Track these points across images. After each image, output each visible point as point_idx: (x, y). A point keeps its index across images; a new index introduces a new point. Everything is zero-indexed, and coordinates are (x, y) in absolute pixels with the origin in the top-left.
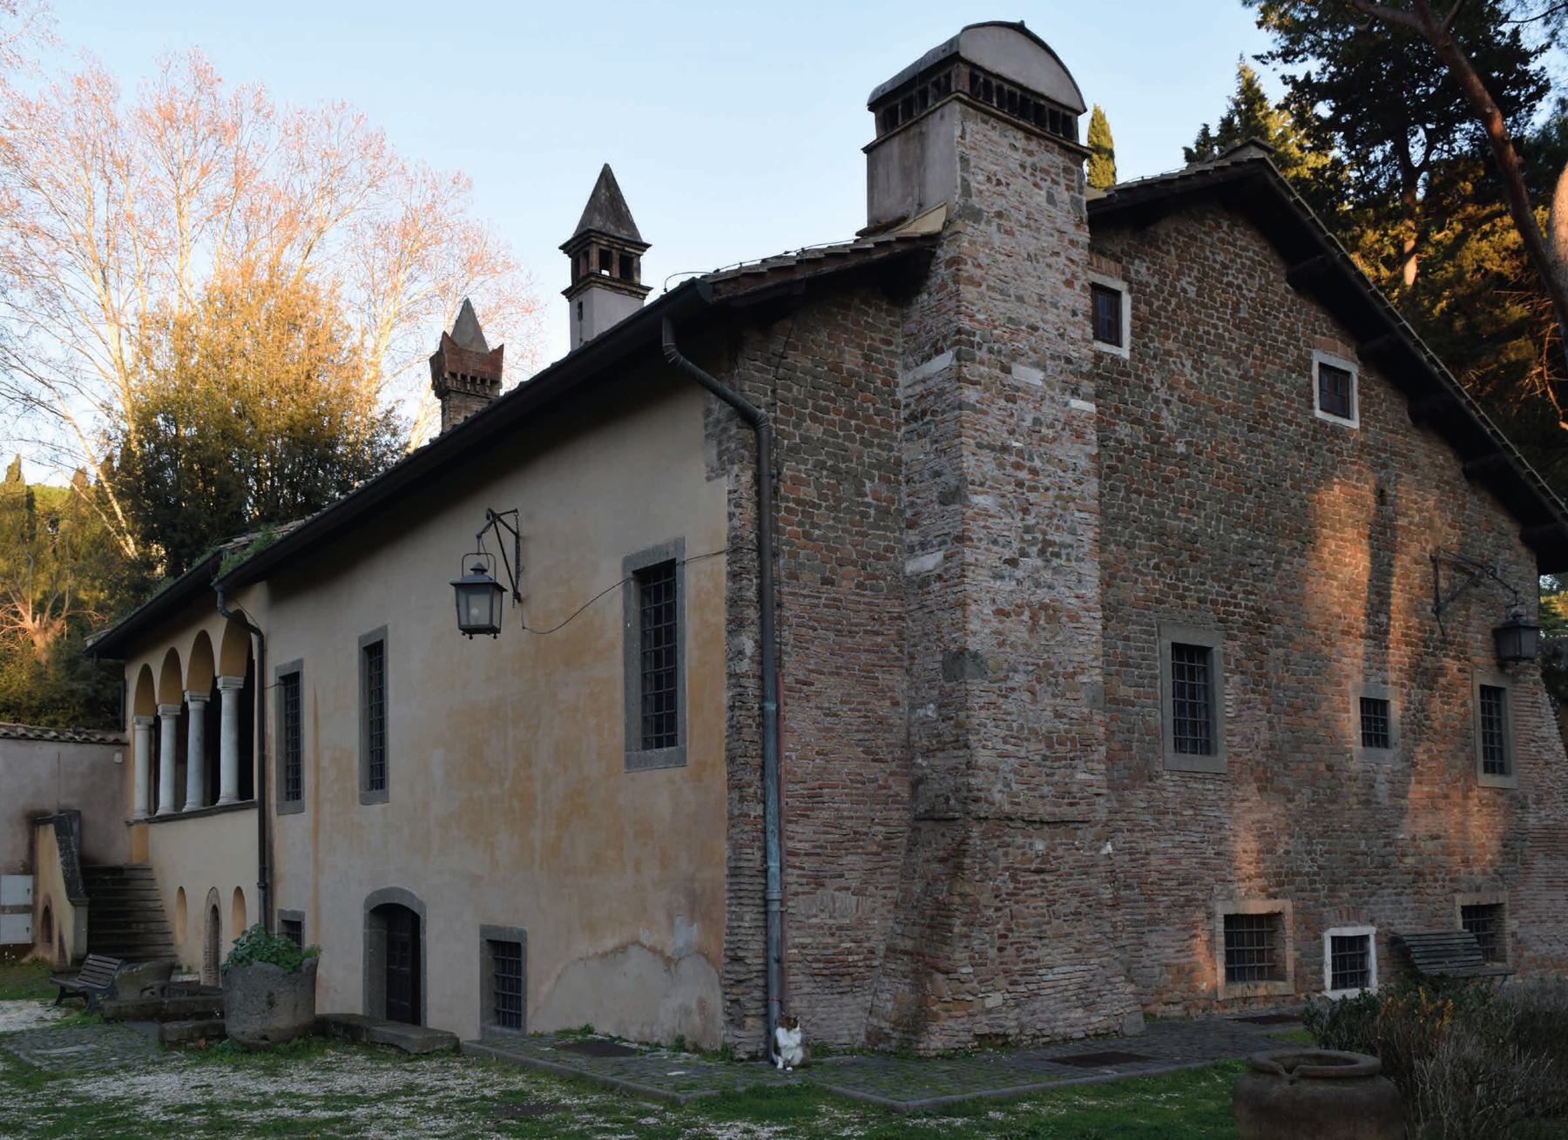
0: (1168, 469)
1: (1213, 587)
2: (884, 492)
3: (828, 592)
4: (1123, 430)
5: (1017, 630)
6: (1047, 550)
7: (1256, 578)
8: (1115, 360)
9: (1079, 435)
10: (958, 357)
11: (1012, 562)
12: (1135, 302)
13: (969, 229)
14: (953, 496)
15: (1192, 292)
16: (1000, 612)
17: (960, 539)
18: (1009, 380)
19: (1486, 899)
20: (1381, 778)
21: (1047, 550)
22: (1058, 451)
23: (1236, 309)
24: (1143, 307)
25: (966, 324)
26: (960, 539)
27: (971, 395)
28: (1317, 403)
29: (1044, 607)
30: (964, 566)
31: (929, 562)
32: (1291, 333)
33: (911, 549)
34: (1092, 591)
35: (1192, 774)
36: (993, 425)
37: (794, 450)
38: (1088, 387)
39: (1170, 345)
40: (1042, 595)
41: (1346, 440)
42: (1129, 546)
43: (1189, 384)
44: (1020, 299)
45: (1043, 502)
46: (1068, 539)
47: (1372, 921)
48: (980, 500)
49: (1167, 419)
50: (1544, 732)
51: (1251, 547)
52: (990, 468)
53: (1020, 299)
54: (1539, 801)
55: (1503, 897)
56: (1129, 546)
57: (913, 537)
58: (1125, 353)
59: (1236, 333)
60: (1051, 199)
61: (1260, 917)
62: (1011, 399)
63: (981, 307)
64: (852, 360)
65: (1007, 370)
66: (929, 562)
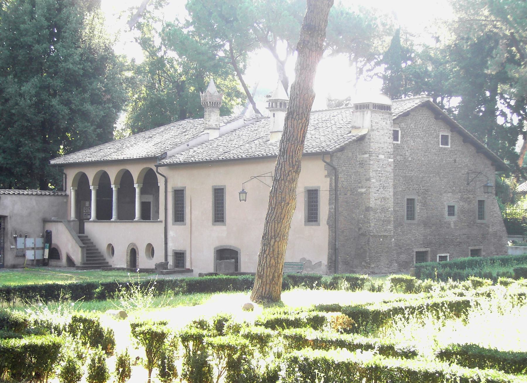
0: (407, 164)
1: (416, 186)
2: (355, 177)
3: (346, 196)
4: (398, 158)
5: (378, 202)
6: (384, 188)
7: (425, 183)
8: (397, 144)
9: (390, 166)
10: (370, 156)
11: (378, 191)
12: (402, 132)
13: (372, 133)
14: (368, 179)
15: (413, 127)
16: (376, 200)
17: (369, 187)
18: (378, 158)
19: (477, 248)
20: (452, 222)
21: (384, 188)
22: (386, 169)
23: (423, 128)
24: (403, 132)
25: (371, 150)
26: (369, 187)
27: (372, 162)
28: (440, 144)
29: (383, 198)
30: (370, 192)
31: (363, 190)
32: (435, 130)
33: (359, 187)
34: (392, 194)
35: (410, 224)
36: (375, 167)
37: (341, 172)
38: (392, 156)
39: (408, 139)
40: (383, 196)
41: (447, 150)
42: (399, 180)
43: (412, 146)
44: (380, 143)
45: (383, 179)
46: (388, 185)
47: (448, 253)
48: (373, 180)
49: (407, 154)
50: (495, 209)
51: (424, 177)
52: (375, 175)
53: (380, 143)
54: (493, 225)
55: (482, 247)
56: (399, 180)
57: (360, 185)
58: (399, 142)
59: (423, 133)
60: (386, 123)
61: (423, 252)
62: (378, 162)
63: (374, 146)
64: (350, 155)
65: (378, 157)
66: (363, 190)
